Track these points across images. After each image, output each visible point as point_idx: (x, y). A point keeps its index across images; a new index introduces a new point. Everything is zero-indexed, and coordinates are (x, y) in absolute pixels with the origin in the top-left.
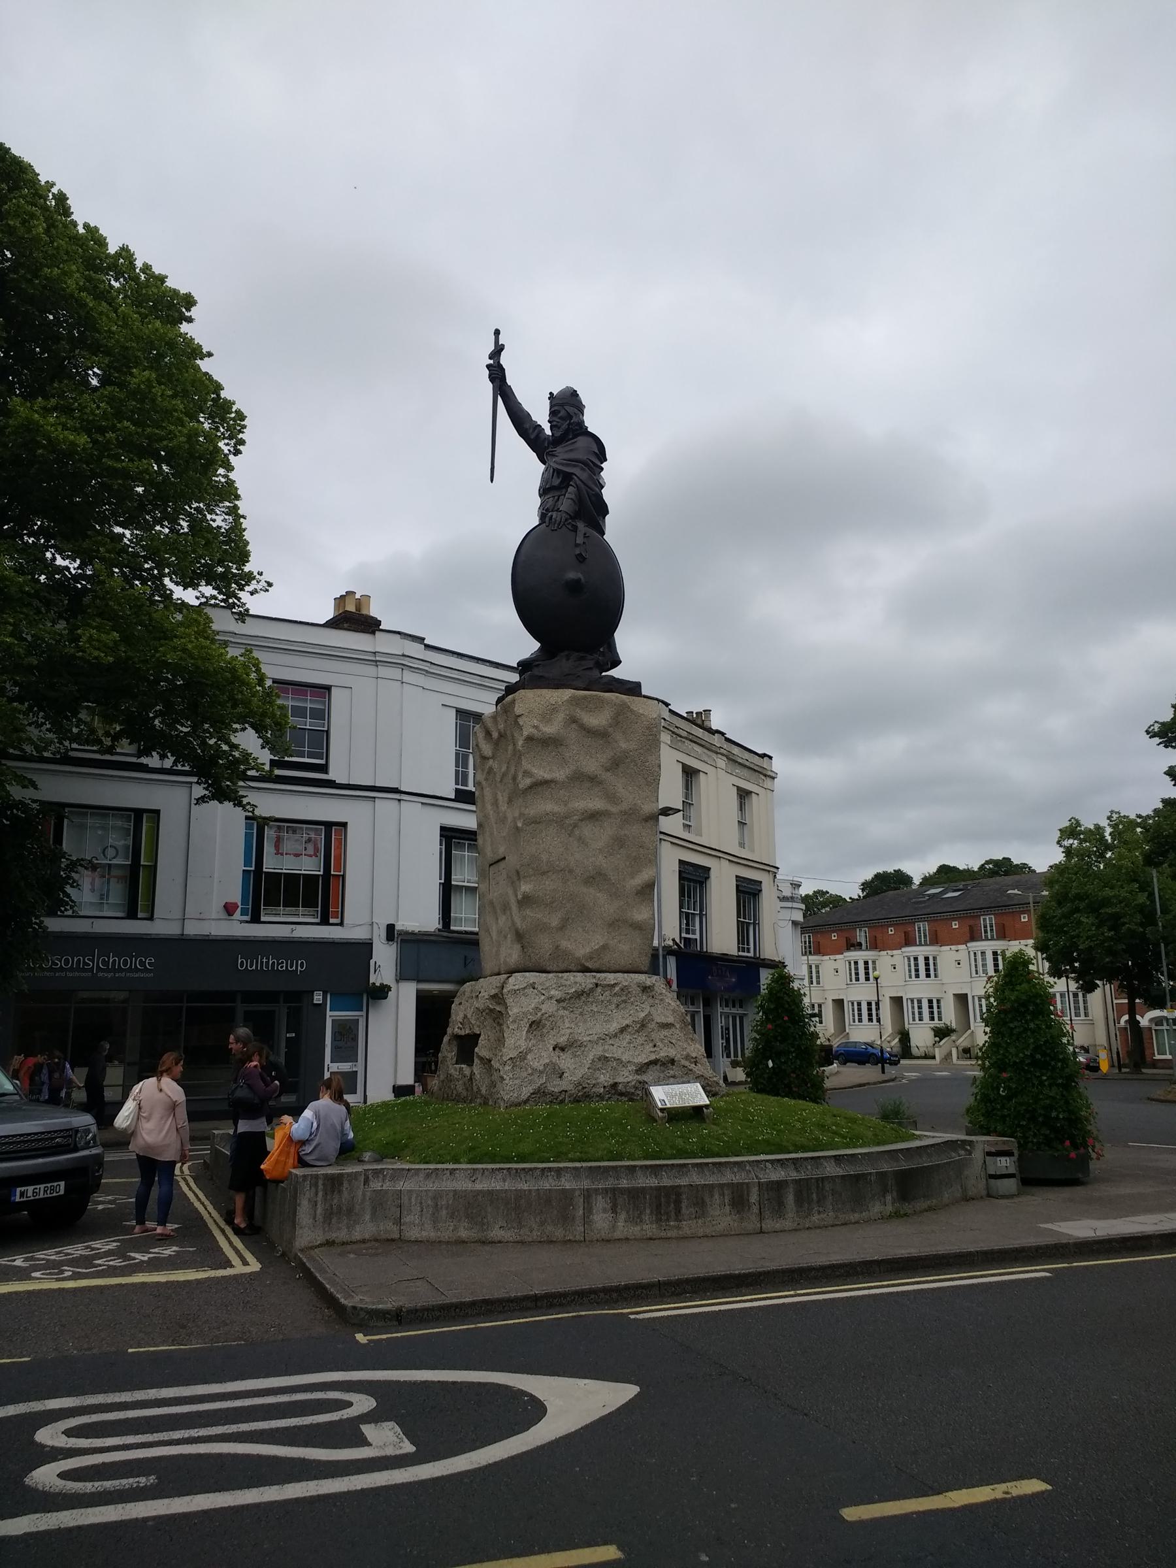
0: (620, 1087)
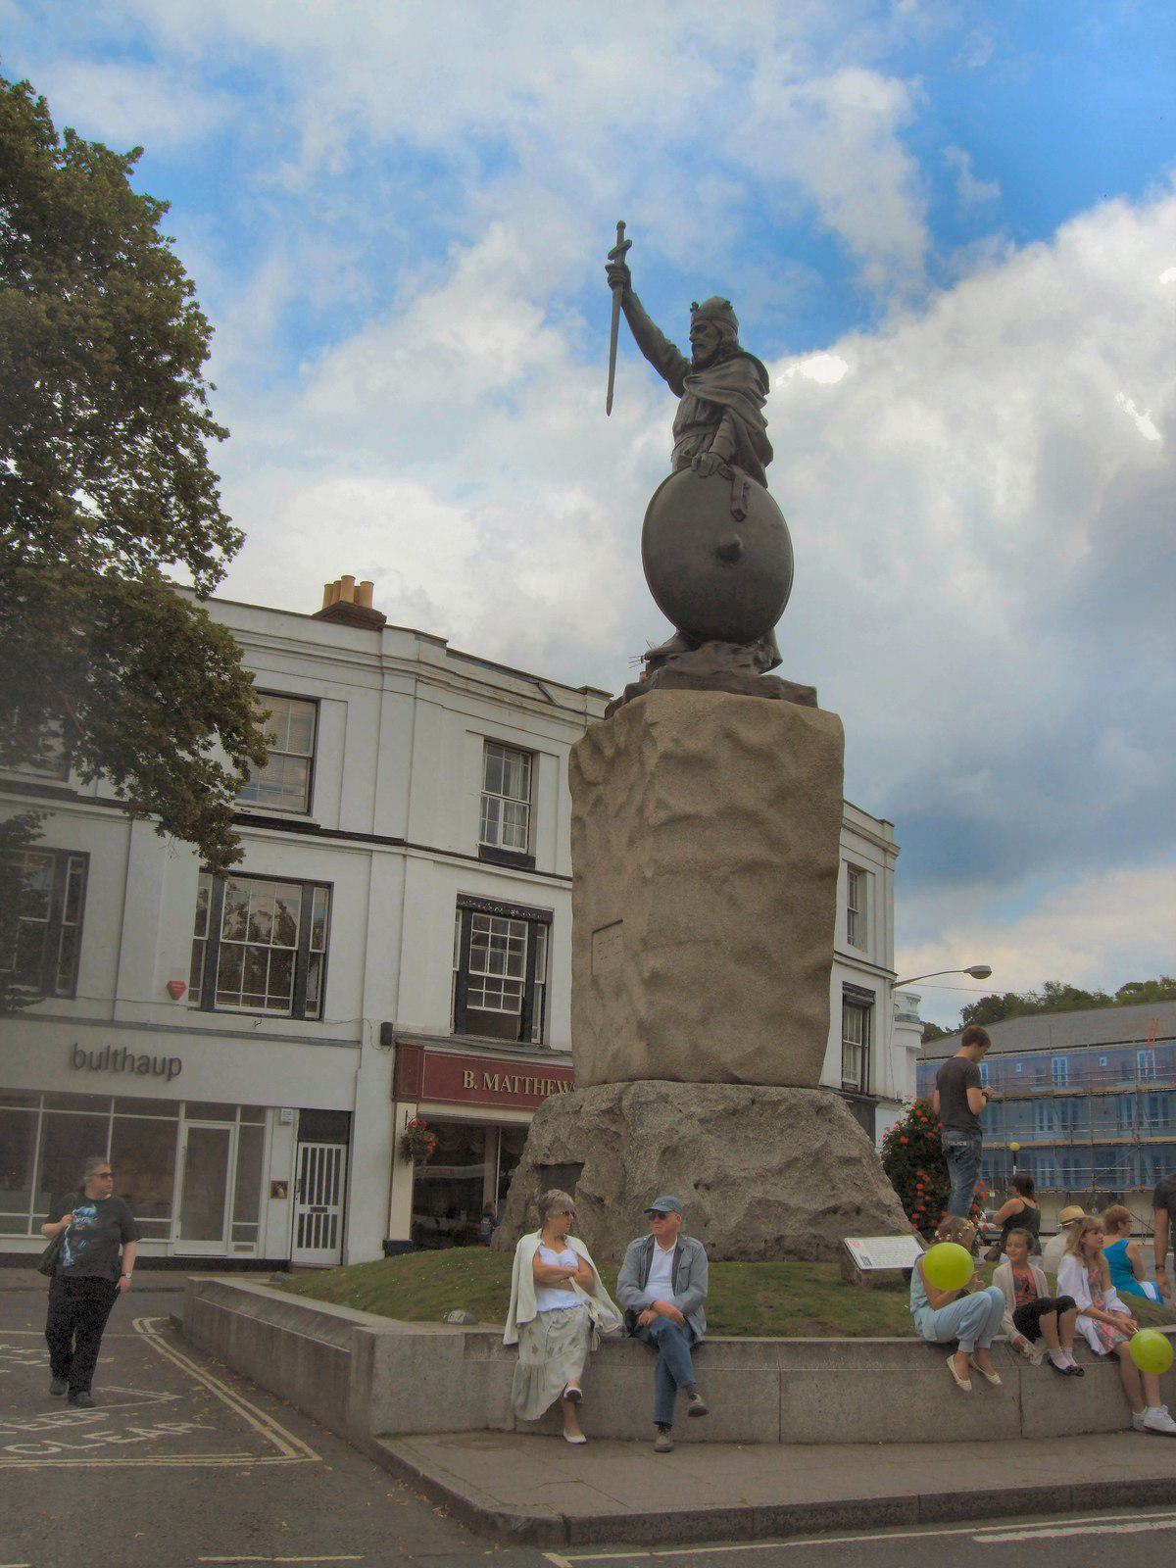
0: (787, 1243)
